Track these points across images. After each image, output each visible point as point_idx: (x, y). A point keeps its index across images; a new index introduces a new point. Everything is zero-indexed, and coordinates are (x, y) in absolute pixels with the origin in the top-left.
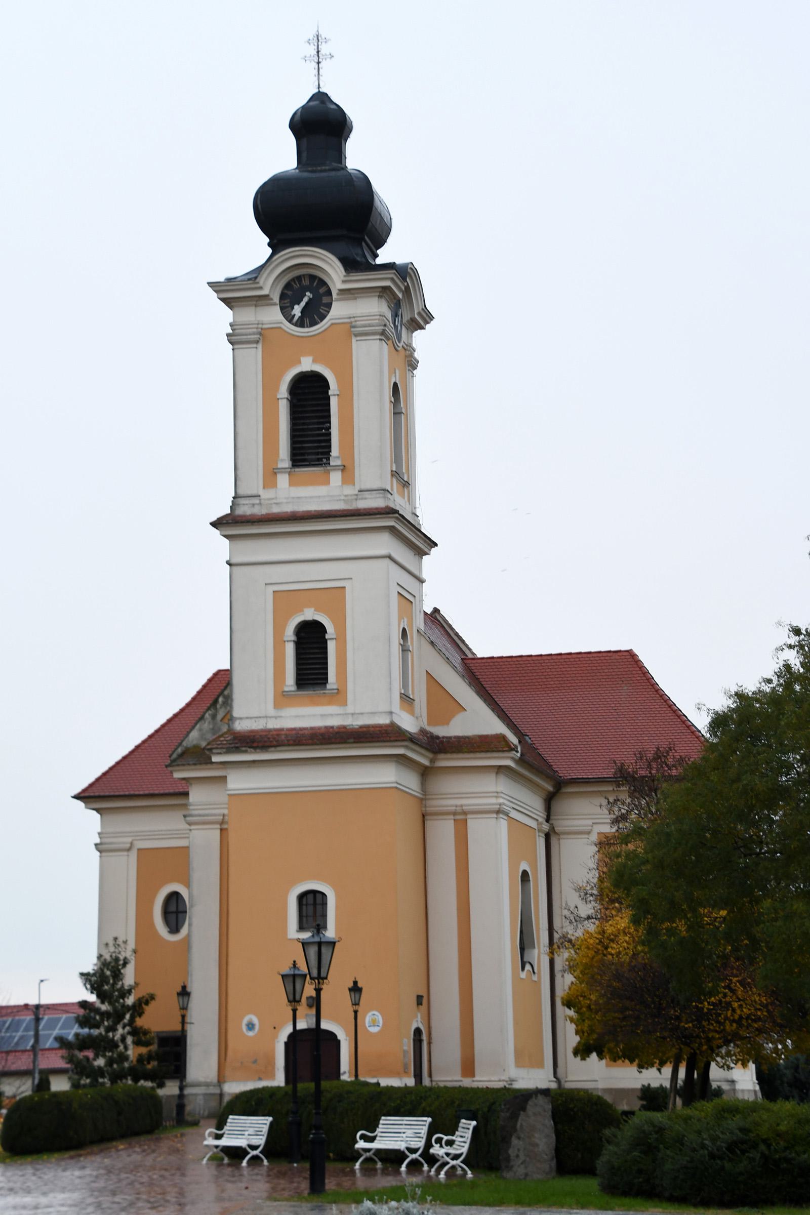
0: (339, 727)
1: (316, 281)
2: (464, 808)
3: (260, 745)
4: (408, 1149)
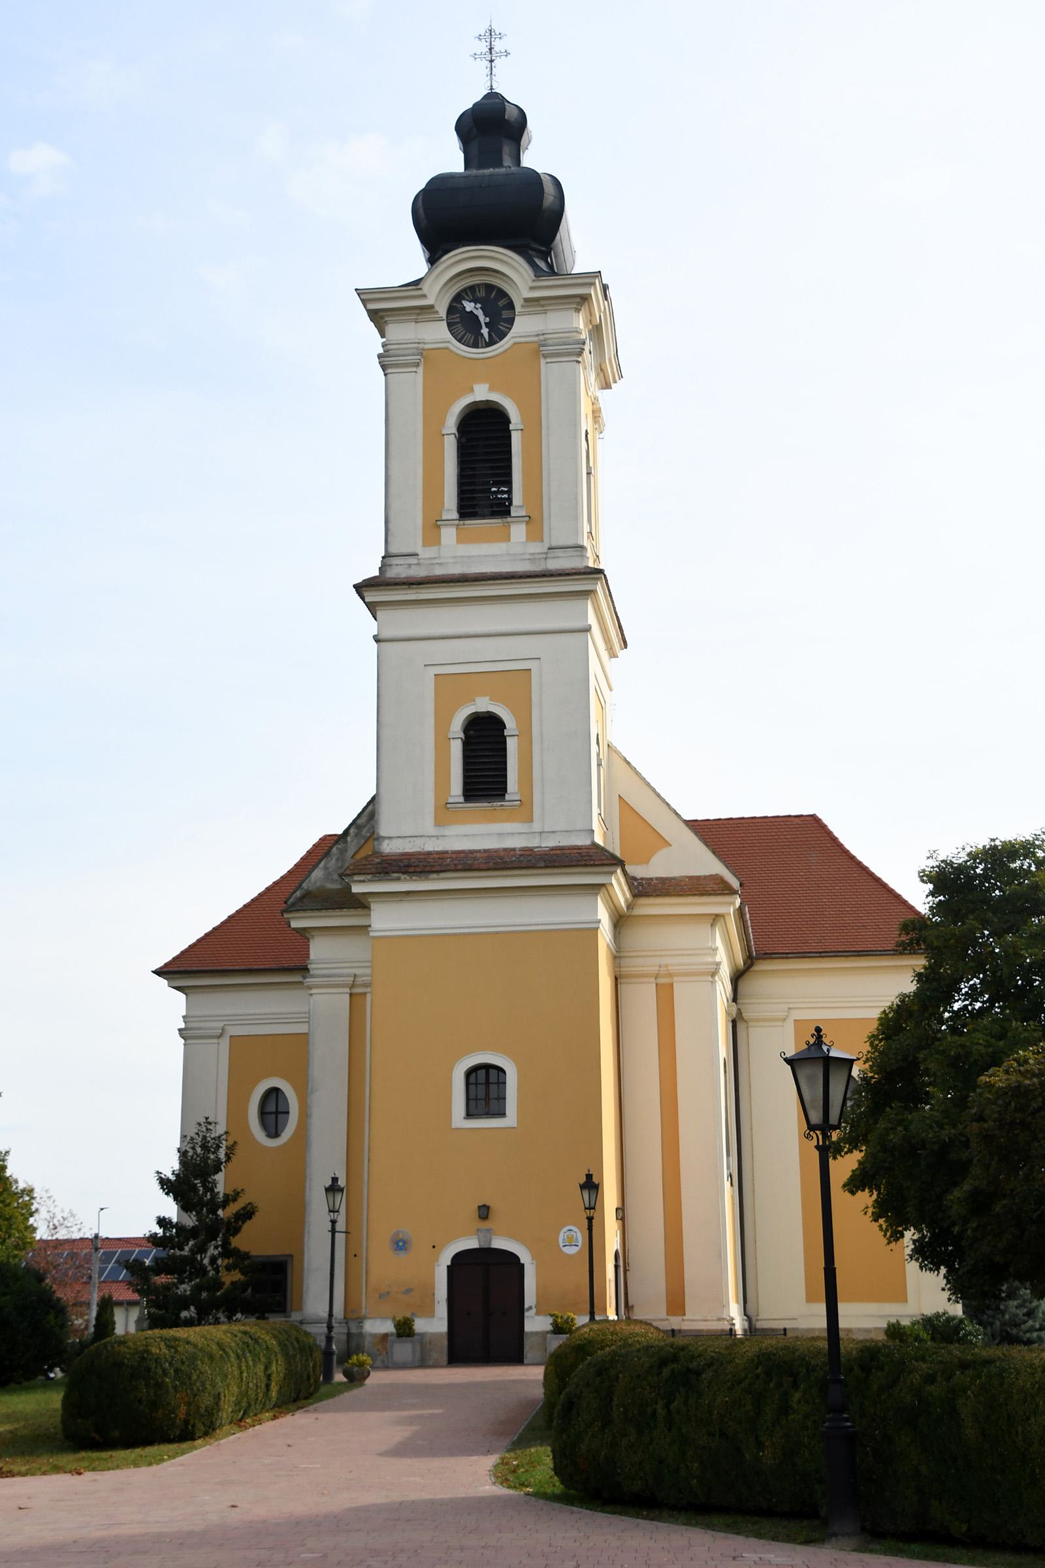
0: (523, 849)
2: (670, 968)
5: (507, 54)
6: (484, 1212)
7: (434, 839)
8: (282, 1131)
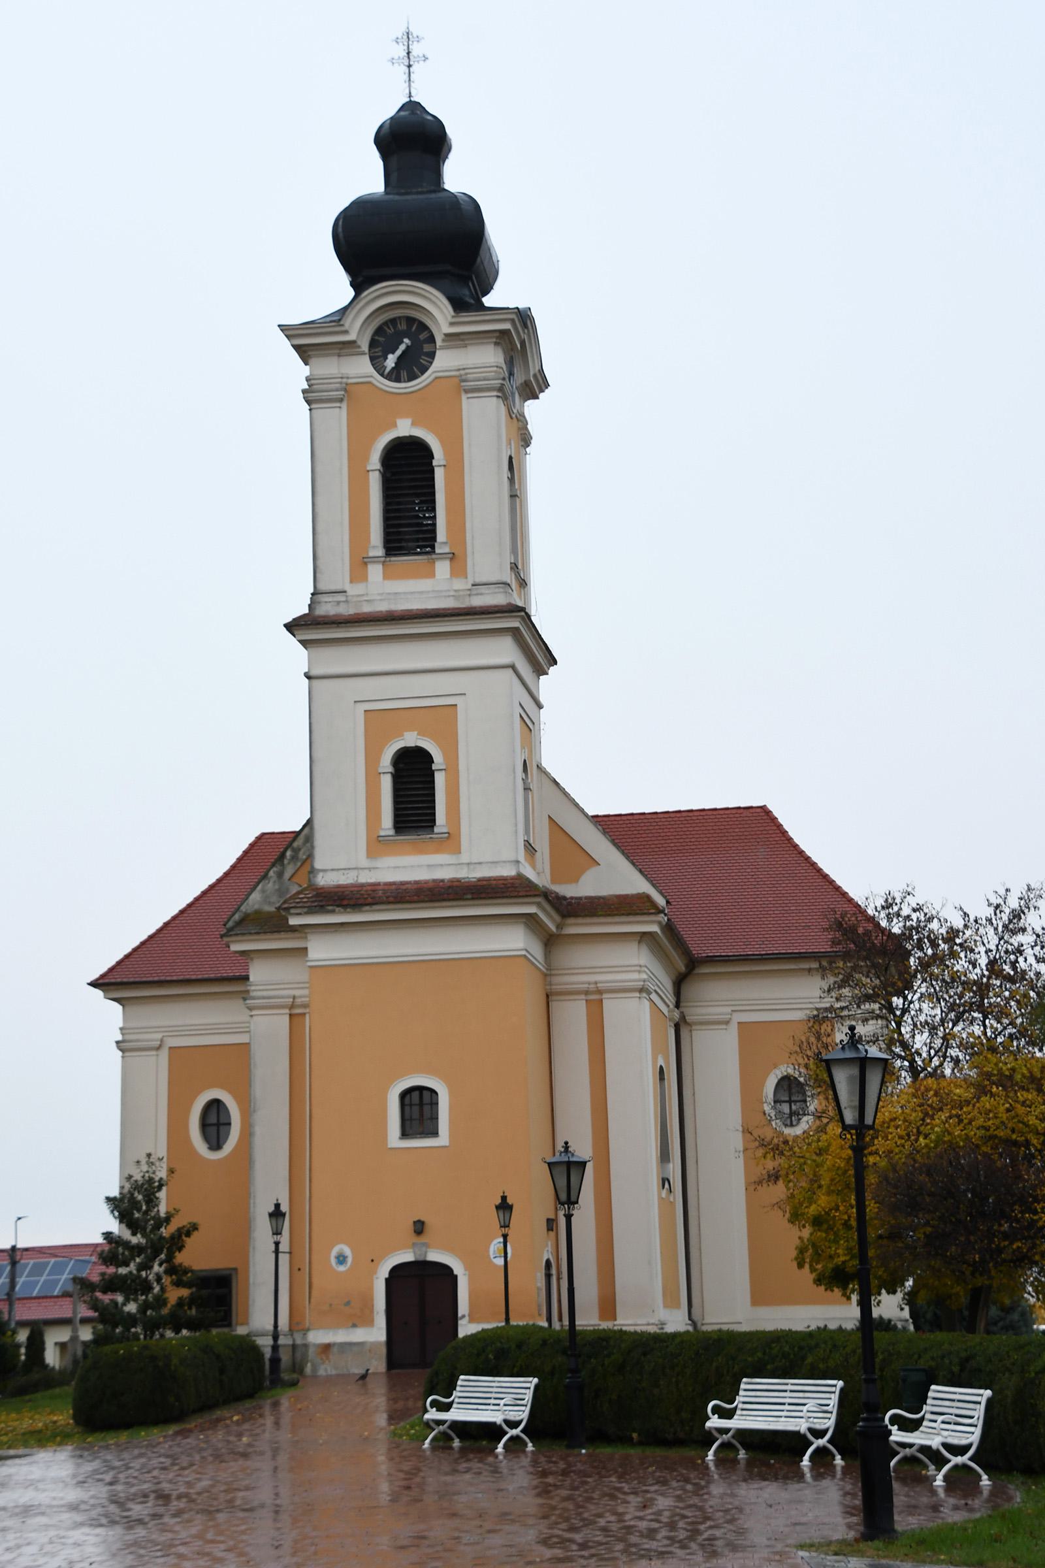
0: (452, 881)
1: (415, 325)
3: (352, 902)
4: (810, 1430)
5: (426, 59)
6: (419, 1228)
7: (367, 871)
8: (225, 1142)
